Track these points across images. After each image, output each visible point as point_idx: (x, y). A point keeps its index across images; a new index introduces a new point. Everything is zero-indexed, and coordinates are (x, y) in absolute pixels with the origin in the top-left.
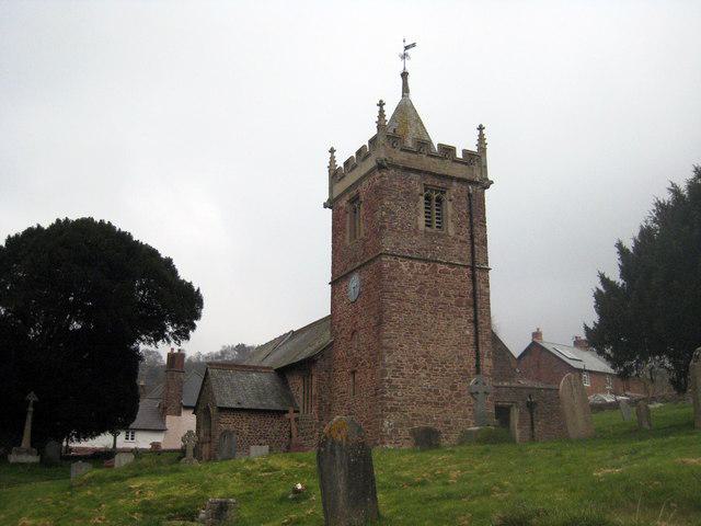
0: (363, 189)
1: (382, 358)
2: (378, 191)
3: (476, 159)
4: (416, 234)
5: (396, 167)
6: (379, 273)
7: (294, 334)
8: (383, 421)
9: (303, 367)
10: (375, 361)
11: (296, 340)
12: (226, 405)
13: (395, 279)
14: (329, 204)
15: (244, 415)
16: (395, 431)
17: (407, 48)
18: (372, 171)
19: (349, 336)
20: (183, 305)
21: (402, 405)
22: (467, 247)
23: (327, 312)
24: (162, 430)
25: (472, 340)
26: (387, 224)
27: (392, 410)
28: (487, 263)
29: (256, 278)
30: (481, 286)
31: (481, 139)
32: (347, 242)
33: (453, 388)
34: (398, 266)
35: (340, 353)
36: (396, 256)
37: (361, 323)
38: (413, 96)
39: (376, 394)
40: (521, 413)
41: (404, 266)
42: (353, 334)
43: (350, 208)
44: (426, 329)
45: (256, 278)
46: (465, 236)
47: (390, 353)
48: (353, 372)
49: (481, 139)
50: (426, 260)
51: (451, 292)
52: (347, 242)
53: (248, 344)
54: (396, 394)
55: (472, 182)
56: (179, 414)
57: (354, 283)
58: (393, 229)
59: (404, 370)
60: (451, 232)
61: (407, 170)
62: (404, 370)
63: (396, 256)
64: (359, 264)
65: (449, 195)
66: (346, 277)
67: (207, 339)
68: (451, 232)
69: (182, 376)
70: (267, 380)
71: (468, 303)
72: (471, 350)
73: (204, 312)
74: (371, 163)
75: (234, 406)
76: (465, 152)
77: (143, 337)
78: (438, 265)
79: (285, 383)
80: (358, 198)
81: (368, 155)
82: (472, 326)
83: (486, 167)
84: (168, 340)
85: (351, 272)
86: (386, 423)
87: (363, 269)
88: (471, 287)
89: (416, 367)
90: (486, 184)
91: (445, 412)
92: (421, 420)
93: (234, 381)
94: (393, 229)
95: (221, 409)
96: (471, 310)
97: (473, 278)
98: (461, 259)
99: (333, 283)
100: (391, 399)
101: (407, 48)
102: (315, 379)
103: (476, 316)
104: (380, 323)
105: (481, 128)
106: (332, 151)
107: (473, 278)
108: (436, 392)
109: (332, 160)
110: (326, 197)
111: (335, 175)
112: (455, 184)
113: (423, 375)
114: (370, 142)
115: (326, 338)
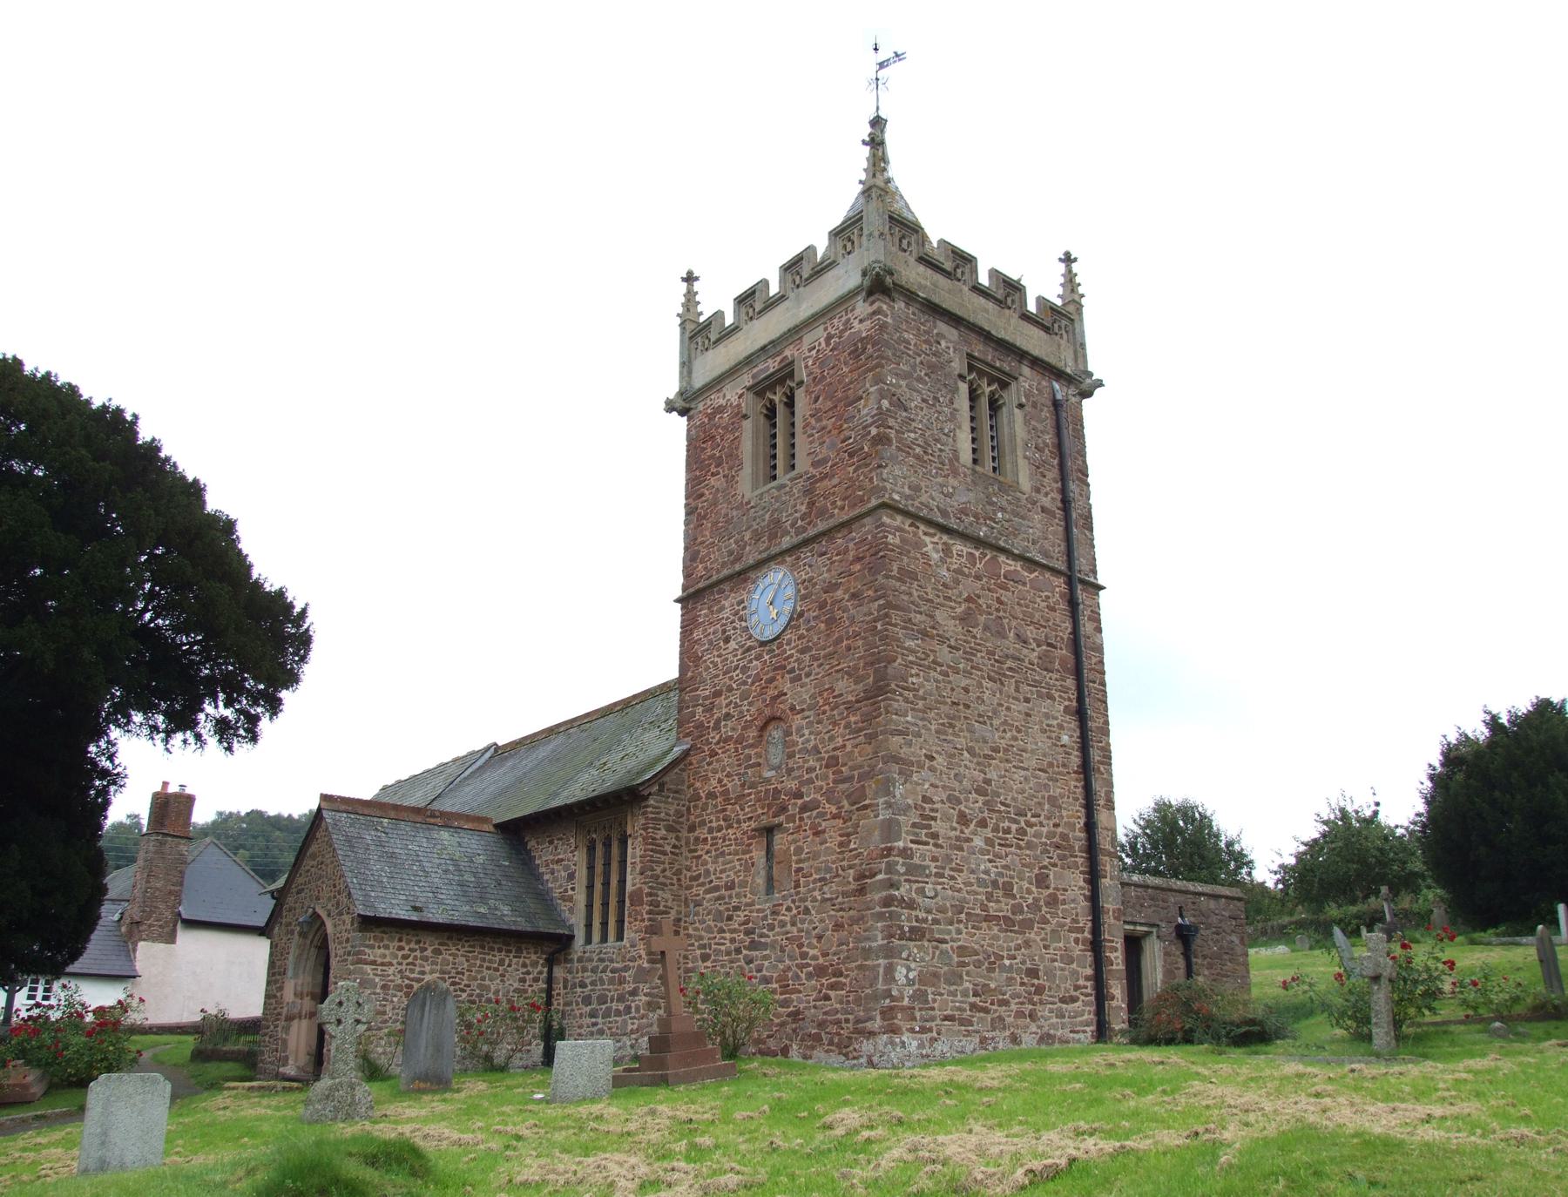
0: (803, 356)
1: (886, 788)
2: (864, 354)
3: (1062, 319)
4: (955, 473)
5: (910, 296)
6: (875, 557)
7: (498, 754)
8: (890, 970)
9: (603, 816)
10: (856, 798)
11: (543, 752)
12: (384, 910)
13: (913, 576)
14: (682, 405)
15: (430, 943)
16: (920, 996)
17: (882, 65)
18: (845, 300)
19: (752, 733)
20: (239, 646)
21: (936, 922)
22: (1057, 528)
23: (668, 670)
24: (126, 977)
25: (1075, 760)
26: (892, 434)
27: (917, 934)
28: (1094, 572)
29: (466, 582)
30: (1087, 627)
31: (1070, 282)
32: (745, 486)
33: (1041, 881)
34: (919, 545)
35: (719, 774)
36: (915, 518)
37: (798, 694)
38: (900, 172)
39: (861, 891)
40: (1167, 954)
41: (931, 544)
42: (763, 728)
43: (750, 404)
44: (982, 719)
45: (466, 582)
46: (1050, 500)
47: (906, 776)
48: (769, 831)
49: (1070, 282)
50: (978, 542)
51: (1030, 632)
52: (745, 486)
53: (502, 741)
54: (921, 891)
55: (1059, 375)
56: (171, 938)
57: (771, 601)
58: (906, 448)
59: (938, 826)
60: (1025, 483)
61: (934, 310)
62: (938, 826)
63: (915, 518)
64: (786, 542)
65: (1011, 396)
66: (742, 577)
67: (345, 733)
68: (1025, 483)
69: (183, 848)
70: (476, 848)
71: (1063, 662)
72: (1075, 784)
73: (310, 672)
74: (846, 278)
75: (403, 914)
76: (1041, 301)
77: (138, 718)
78: (1002, 558)
79: (525, 861)
80: (791, 375)
81: (821, 270)
82: (1072, 724)
83: (1083, 346)
84: (198, 737)
85: (759, 565)
86: (900, 973)
87: (805, 554)
88: (1068, 625)
89: (963, 819)
90: (1085, 386)
91: (1027, 944)
92: (978, 964)
93: (396, 846)
94: (906, 448)
95: (371, 924)
96: (1070, 682)
97: (1073, 604)
98: (1046, 555)
99: (690, 599)
100: (911, 905)
101: (882, 65)
102: (635, 851)
103: (1080, 699)
104: (878, 691)
105: (1068, 259)
106: (690, 278)
107: (1073, 604)
108: (1008, 893)
109: (690, 300)
110: (672, 388)
111: (699, 333)
112: (1026, 370)
113: (978, 842)
114: (836, 234)
115: (654, 746)
